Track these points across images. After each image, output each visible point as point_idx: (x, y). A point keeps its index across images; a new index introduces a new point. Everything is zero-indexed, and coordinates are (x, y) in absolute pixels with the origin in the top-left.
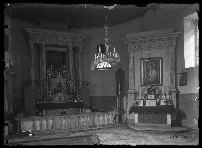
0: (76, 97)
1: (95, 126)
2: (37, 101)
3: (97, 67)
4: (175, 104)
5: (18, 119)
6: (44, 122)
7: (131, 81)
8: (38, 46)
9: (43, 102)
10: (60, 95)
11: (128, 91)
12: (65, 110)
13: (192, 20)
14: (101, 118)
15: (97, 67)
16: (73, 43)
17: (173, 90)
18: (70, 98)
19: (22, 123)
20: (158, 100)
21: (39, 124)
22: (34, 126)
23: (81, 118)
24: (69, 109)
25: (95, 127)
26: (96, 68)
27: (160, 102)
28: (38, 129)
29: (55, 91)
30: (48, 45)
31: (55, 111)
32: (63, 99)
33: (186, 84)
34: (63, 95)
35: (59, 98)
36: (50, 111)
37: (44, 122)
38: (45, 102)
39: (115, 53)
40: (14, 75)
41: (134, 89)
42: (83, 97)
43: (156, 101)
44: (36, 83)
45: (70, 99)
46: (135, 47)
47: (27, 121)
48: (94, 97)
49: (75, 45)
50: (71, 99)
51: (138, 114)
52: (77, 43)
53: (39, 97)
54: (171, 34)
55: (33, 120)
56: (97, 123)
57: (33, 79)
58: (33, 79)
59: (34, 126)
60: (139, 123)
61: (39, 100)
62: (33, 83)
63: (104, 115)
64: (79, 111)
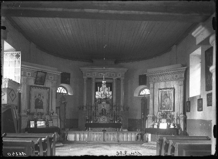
0: (117, 118)
1: (119, 142)
2: (86, 121)
3: (141, 94)
4: (182, 127)
5: (66, 132)
6: (82, 135)
7: (151, 107)
8: (90, 79)
9: (115, 121)
10: (104, 117)
11: (149, 115)
12: (106, 129)
13: (197, 56)
14: (125, 136)
15: (141, 94)
16: (116, 76)
17: (181, 116)
18: (111, 119)
19: (68, 135)
20: (169, 124)
21: (78, 136)
22: (75, 138)
23: (108, 134)
24: (109, 128)
25: (119, 142)
26: (139, 95)
27: (170, 126)
28: (78, 140)
29: (100, 114)
30: (96, 79)
31: (98, 129)
32: (106, 120)
33: (190, 111)
34: (106, 117)
35: (103, 120)
36: (94, 129)
37: (82, 135)
38: (92, 122)
39: (110, 92)
40: (65, 103)
41: (153, 114)
42: (122, 120)
43: (168, 124)
44: (86, 107)
45: (111, 121)
46: (155, 79)
47: (71, 134)
48: (136, 120)
49: (117, 77)
50: (112, 121)
51: (151, 134)
52: (119, 75)
53: (88, 118)
54: (179, 68)
55: (75, 134)
56: (121, 140)
57: (85, 104)
58: (85, 104)
59: (75, 138)
60: (151, 142)
61: (88, 120)
62: (85, 108)
63: (131, 134)
64: (117, 130)
